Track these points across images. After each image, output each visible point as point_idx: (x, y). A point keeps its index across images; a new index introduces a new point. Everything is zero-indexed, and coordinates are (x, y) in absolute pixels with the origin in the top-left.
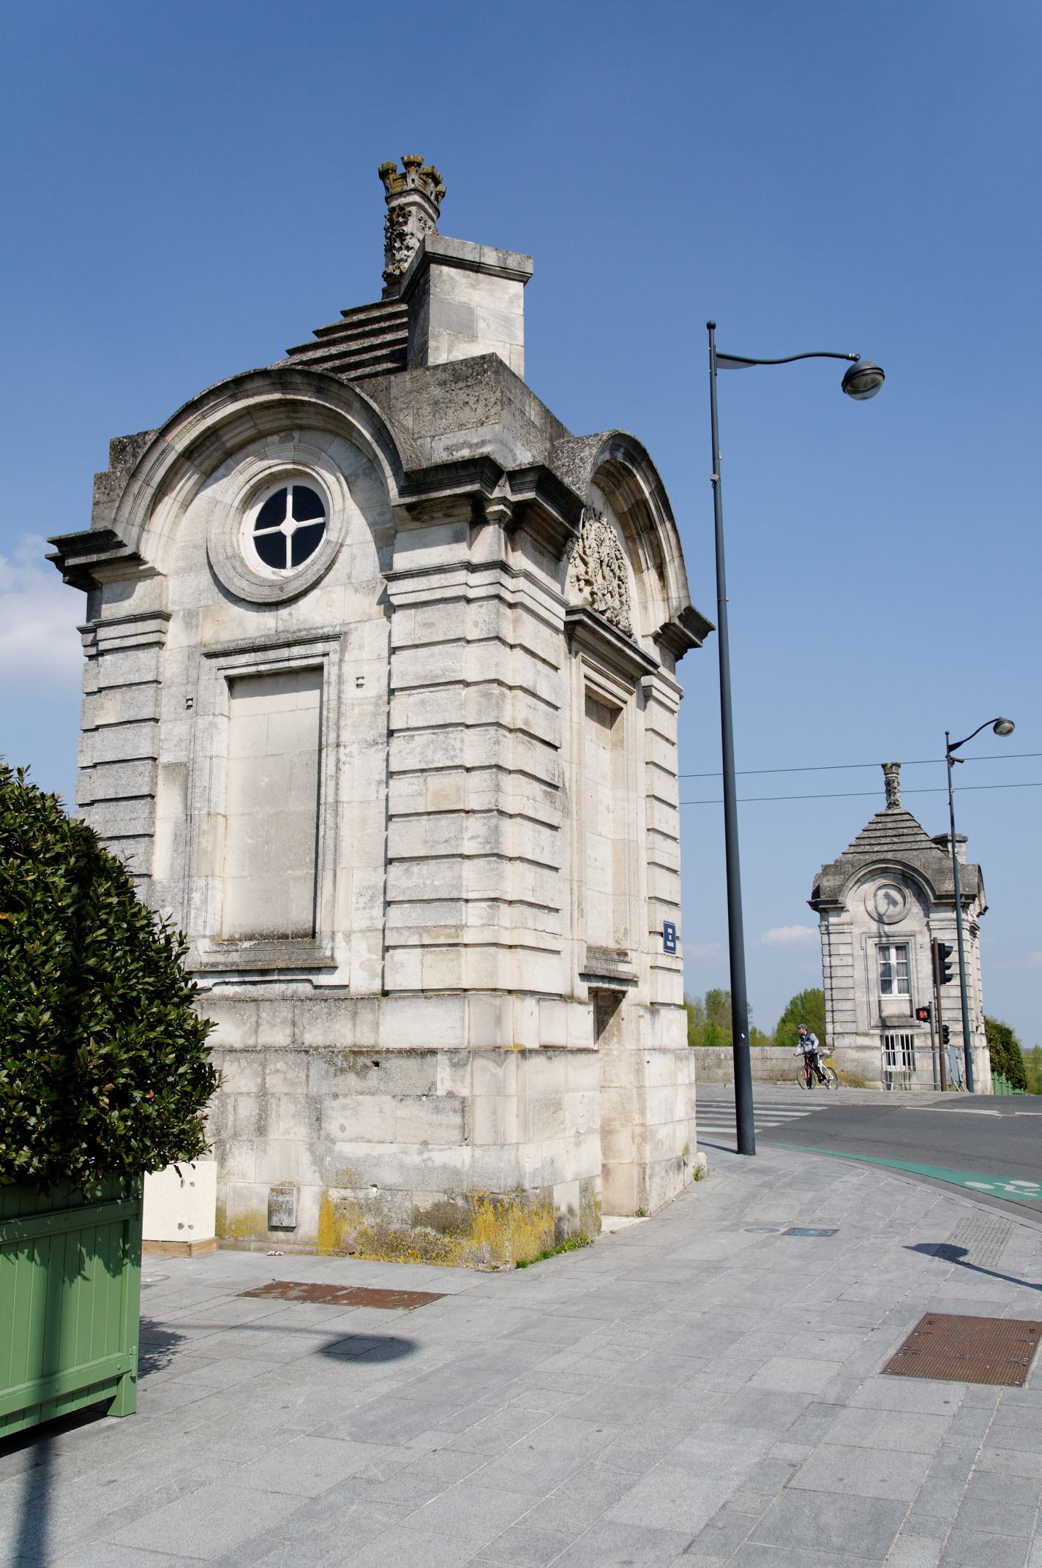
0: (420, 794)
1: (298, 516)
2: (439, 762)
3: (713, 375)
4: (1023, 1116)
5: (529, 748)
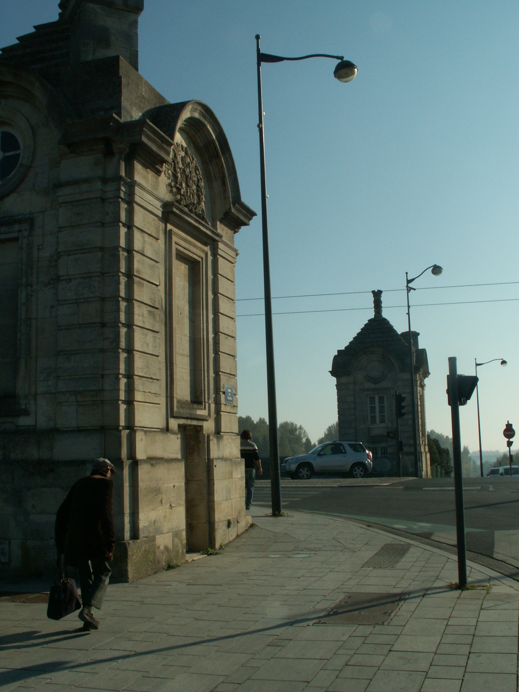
4: (13, 643)
5: (140, 286)
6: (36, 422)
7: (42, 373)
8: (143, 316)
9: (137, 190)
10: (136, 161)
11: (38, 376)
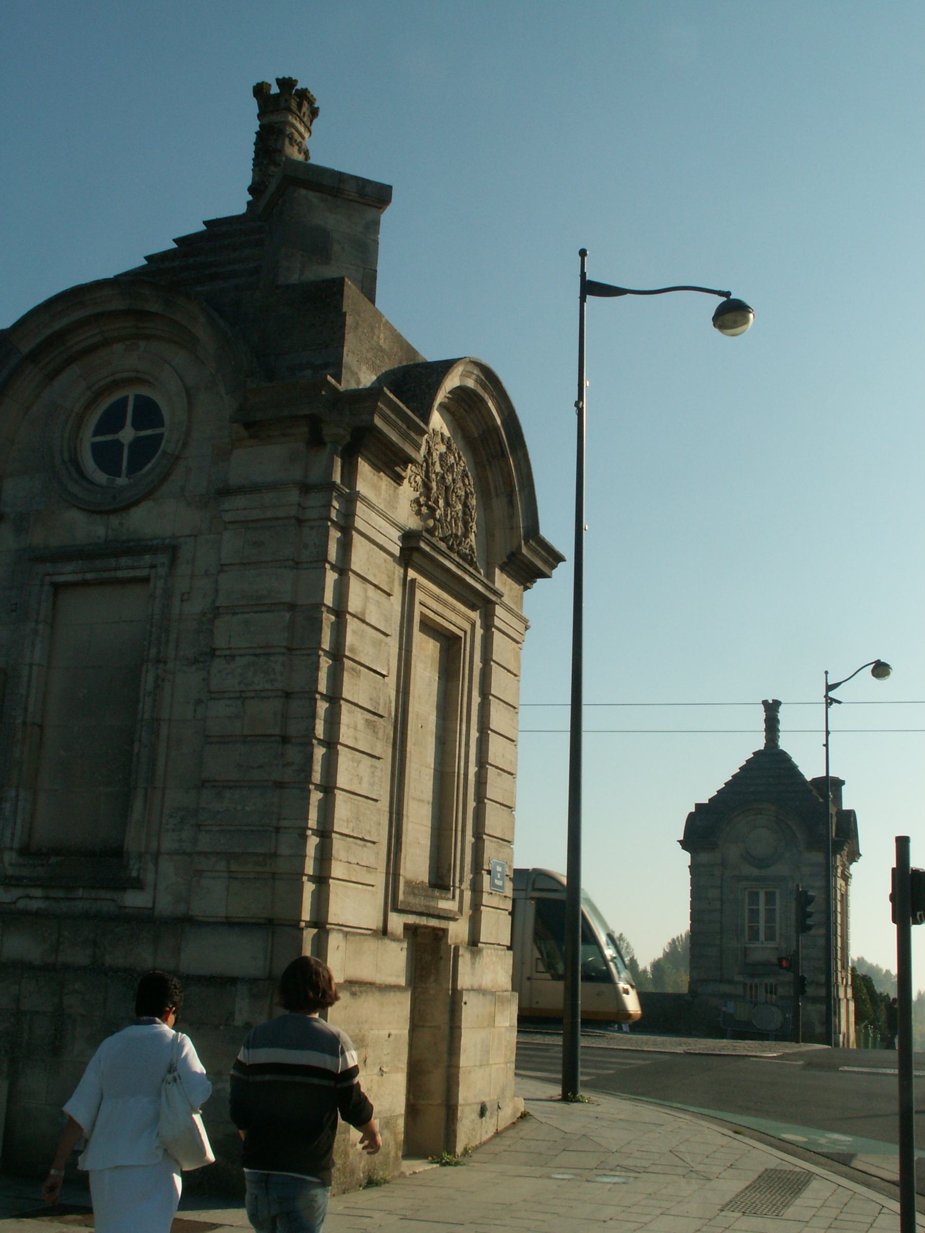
1: (137, 426)
3: (583, 300)
5: (353, 675)
8: (355, 728)
9: (360, 507)
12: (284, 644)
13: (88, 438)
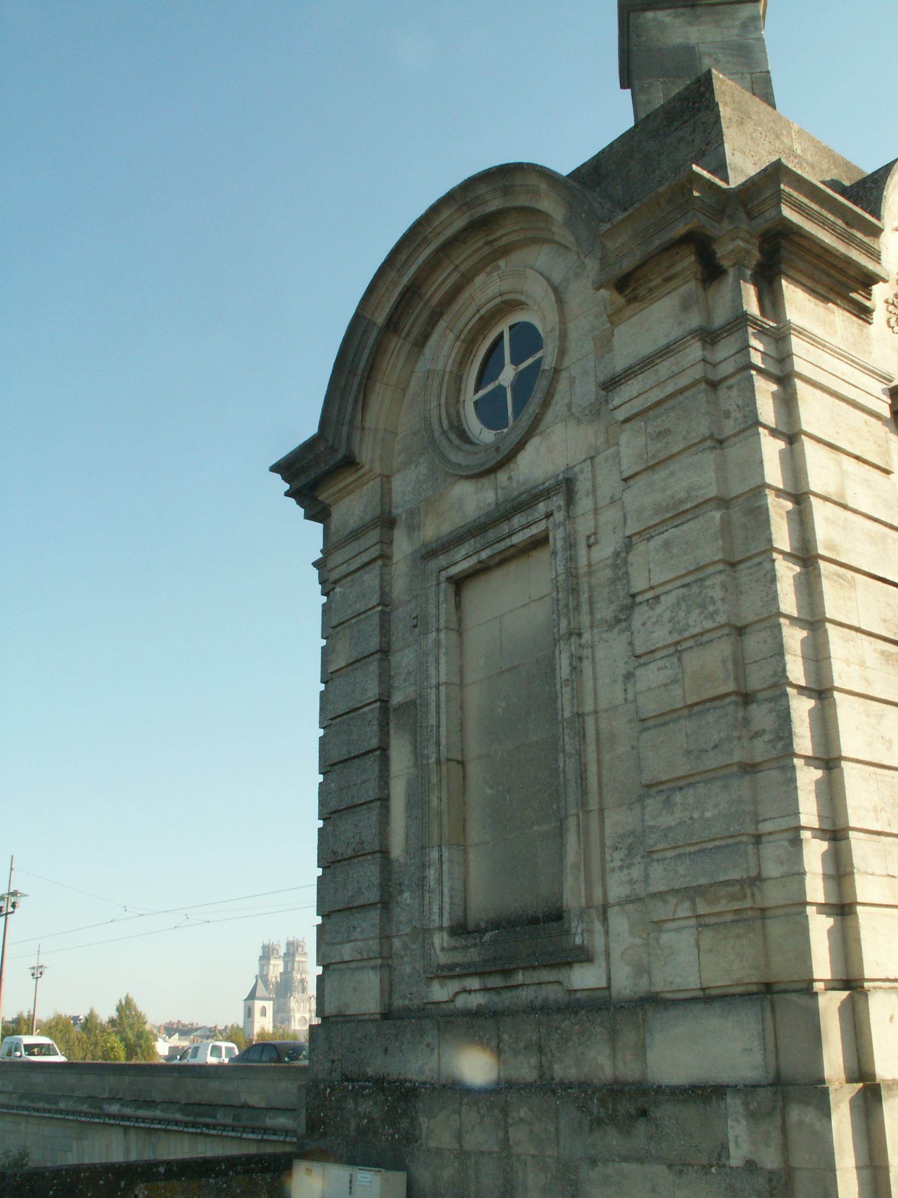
0: (674, 681)
2: (695, 626)
5: (841, 584)
6: (609, 979)
7: (616, 849)
8: (863, 665)
9: (797, 344)
10: (786, 281)
11: (608, 857)
12: (720, 556)
13: (470, 396)
